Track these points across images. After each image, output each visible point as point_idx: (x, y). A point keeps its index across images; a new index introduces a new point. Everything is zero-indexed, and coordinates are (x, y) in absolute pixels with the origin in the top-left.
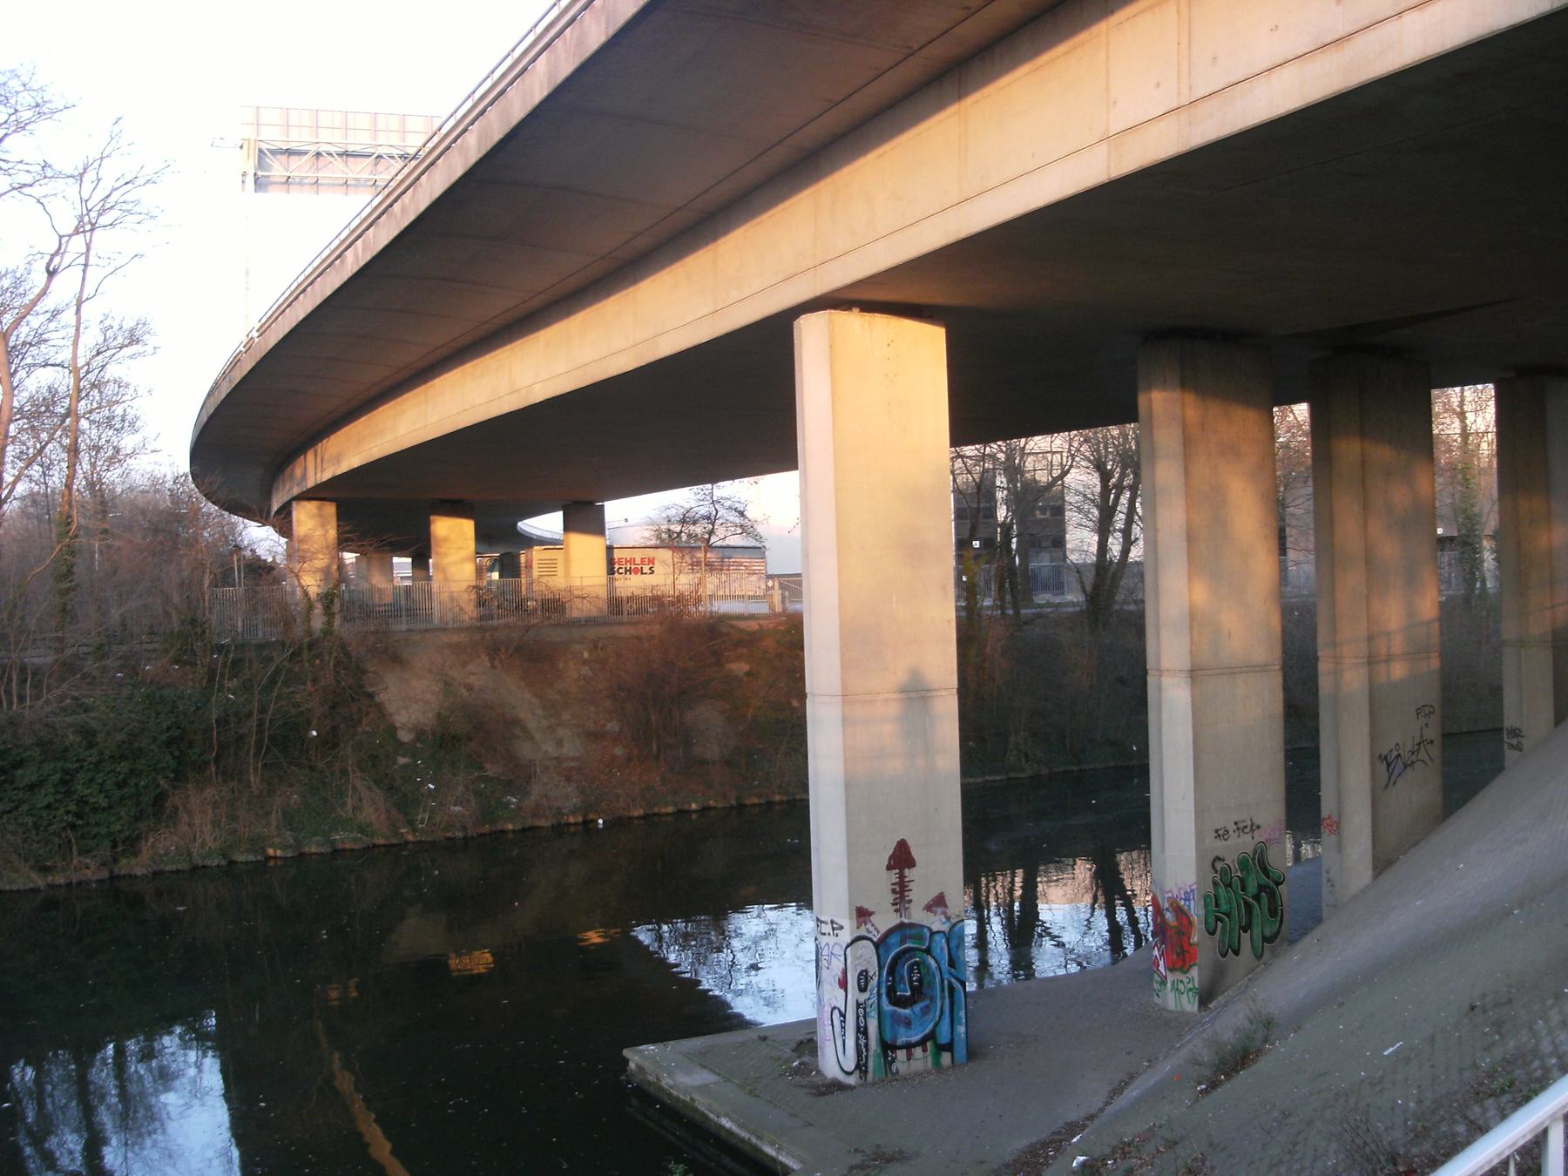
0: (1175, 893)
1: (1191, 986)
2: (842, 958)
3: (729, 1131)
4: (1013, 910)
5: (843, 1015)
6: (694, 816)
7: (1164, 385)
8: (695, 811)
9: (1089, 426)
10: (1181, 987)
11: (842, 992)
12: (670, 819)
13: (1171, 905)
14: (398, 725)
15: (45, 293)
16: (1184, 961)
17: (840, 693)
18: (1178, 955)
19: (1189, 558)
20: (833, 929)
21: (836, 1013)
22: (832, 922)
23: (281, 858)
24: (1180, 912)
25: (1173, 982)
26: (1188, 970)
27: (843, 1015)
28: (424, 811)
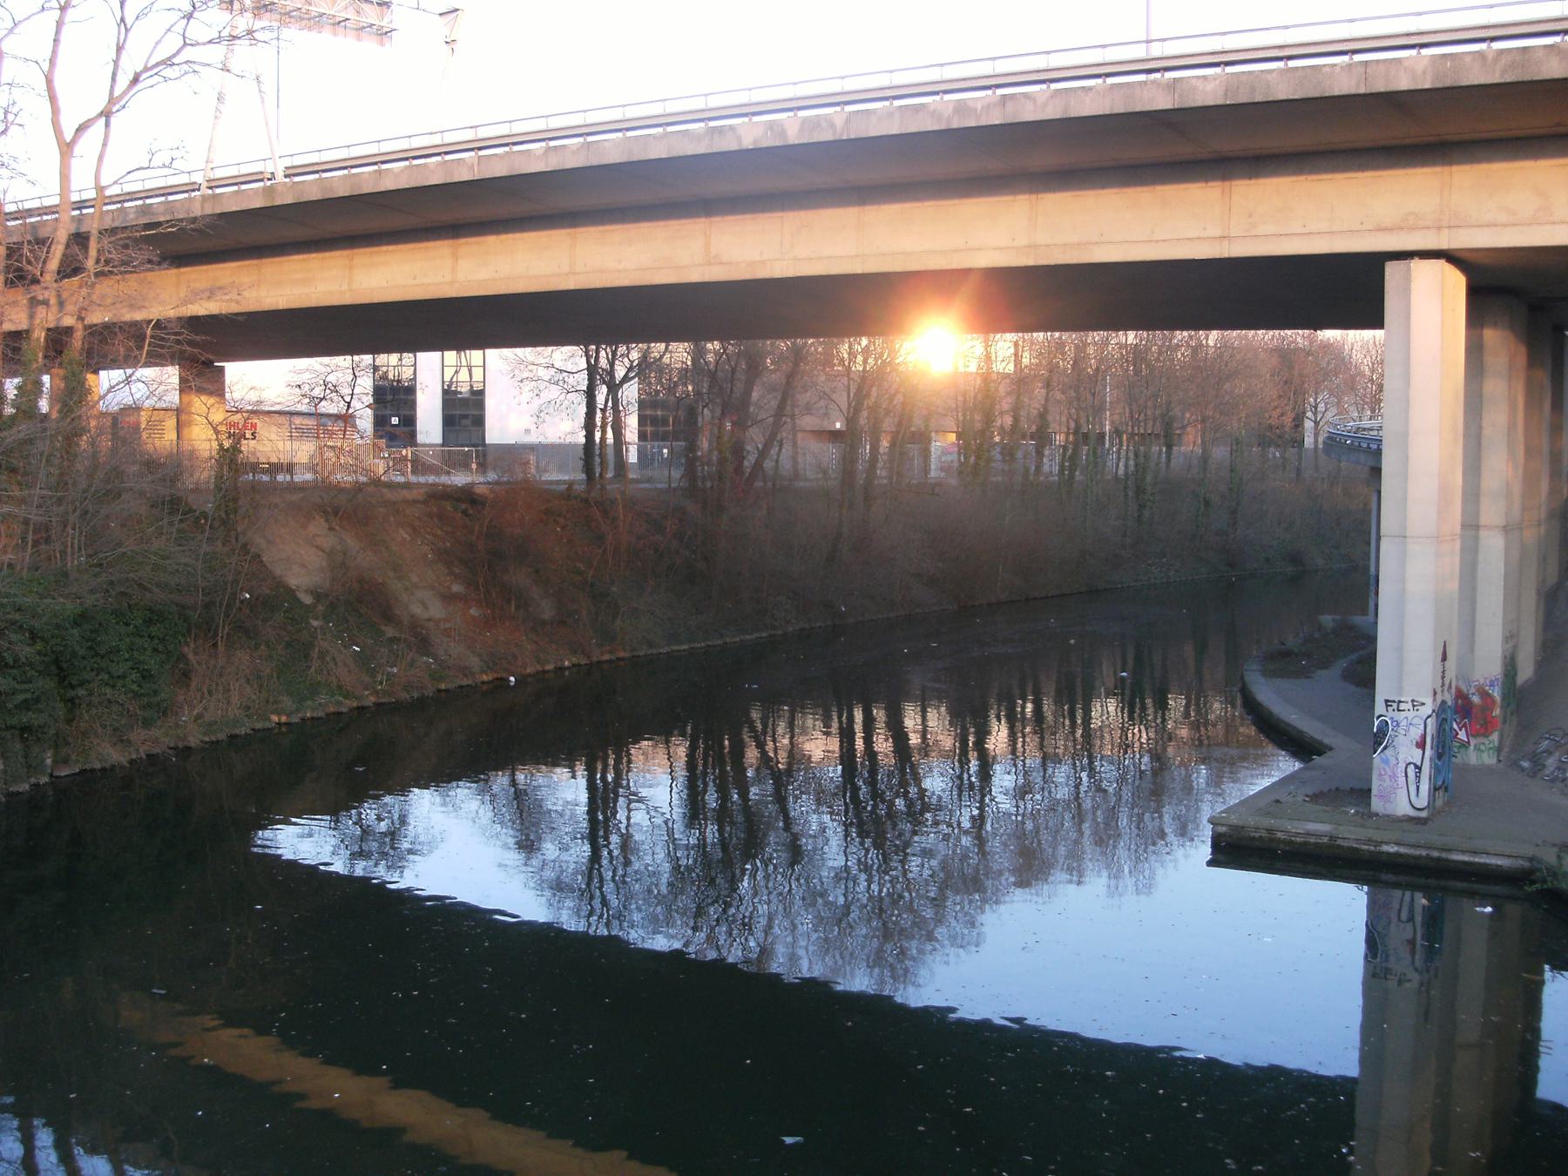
0: (1482, 681)
1: (1491, 746)
2: (1422, 727)
3: (1397, 854)
4: (908, 747)
5: (1419, 768)
6: (567, 673)
7: (1495, 325)
8: (568, 668)
9: (1147, 328)
10: (1482, 747)
11: (1420, 751)
12: (552, 675)
13: (1478, 690)
14: (294, 587)
15: (77, 130)
16: (1486, 729)
17: (1408, 540)
18: (1482, 725)
19: (1509, 447)
20: (1414, 706)
21: (1411, 769)
22: (1413, 701)
23: (286, 724)
24: (1485, 695)
25: (1475, 745)
26: (1490, 734)
27: (1419, 768)
28: (383, 674)
